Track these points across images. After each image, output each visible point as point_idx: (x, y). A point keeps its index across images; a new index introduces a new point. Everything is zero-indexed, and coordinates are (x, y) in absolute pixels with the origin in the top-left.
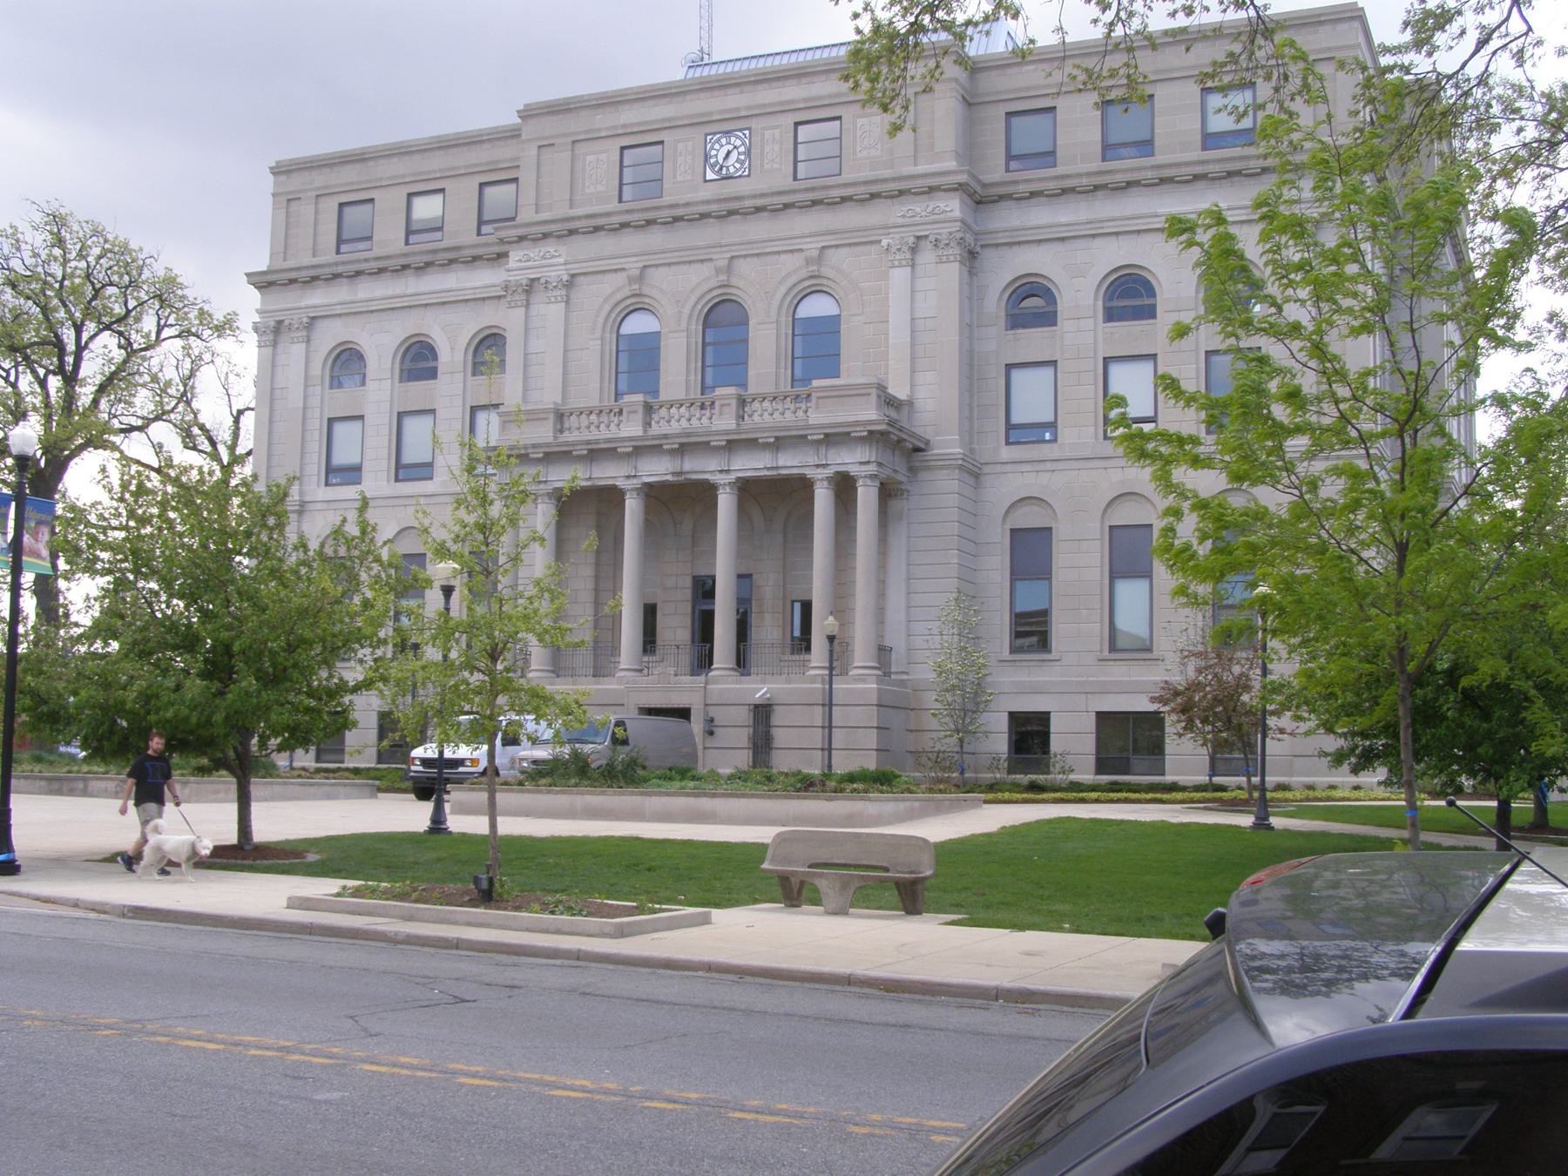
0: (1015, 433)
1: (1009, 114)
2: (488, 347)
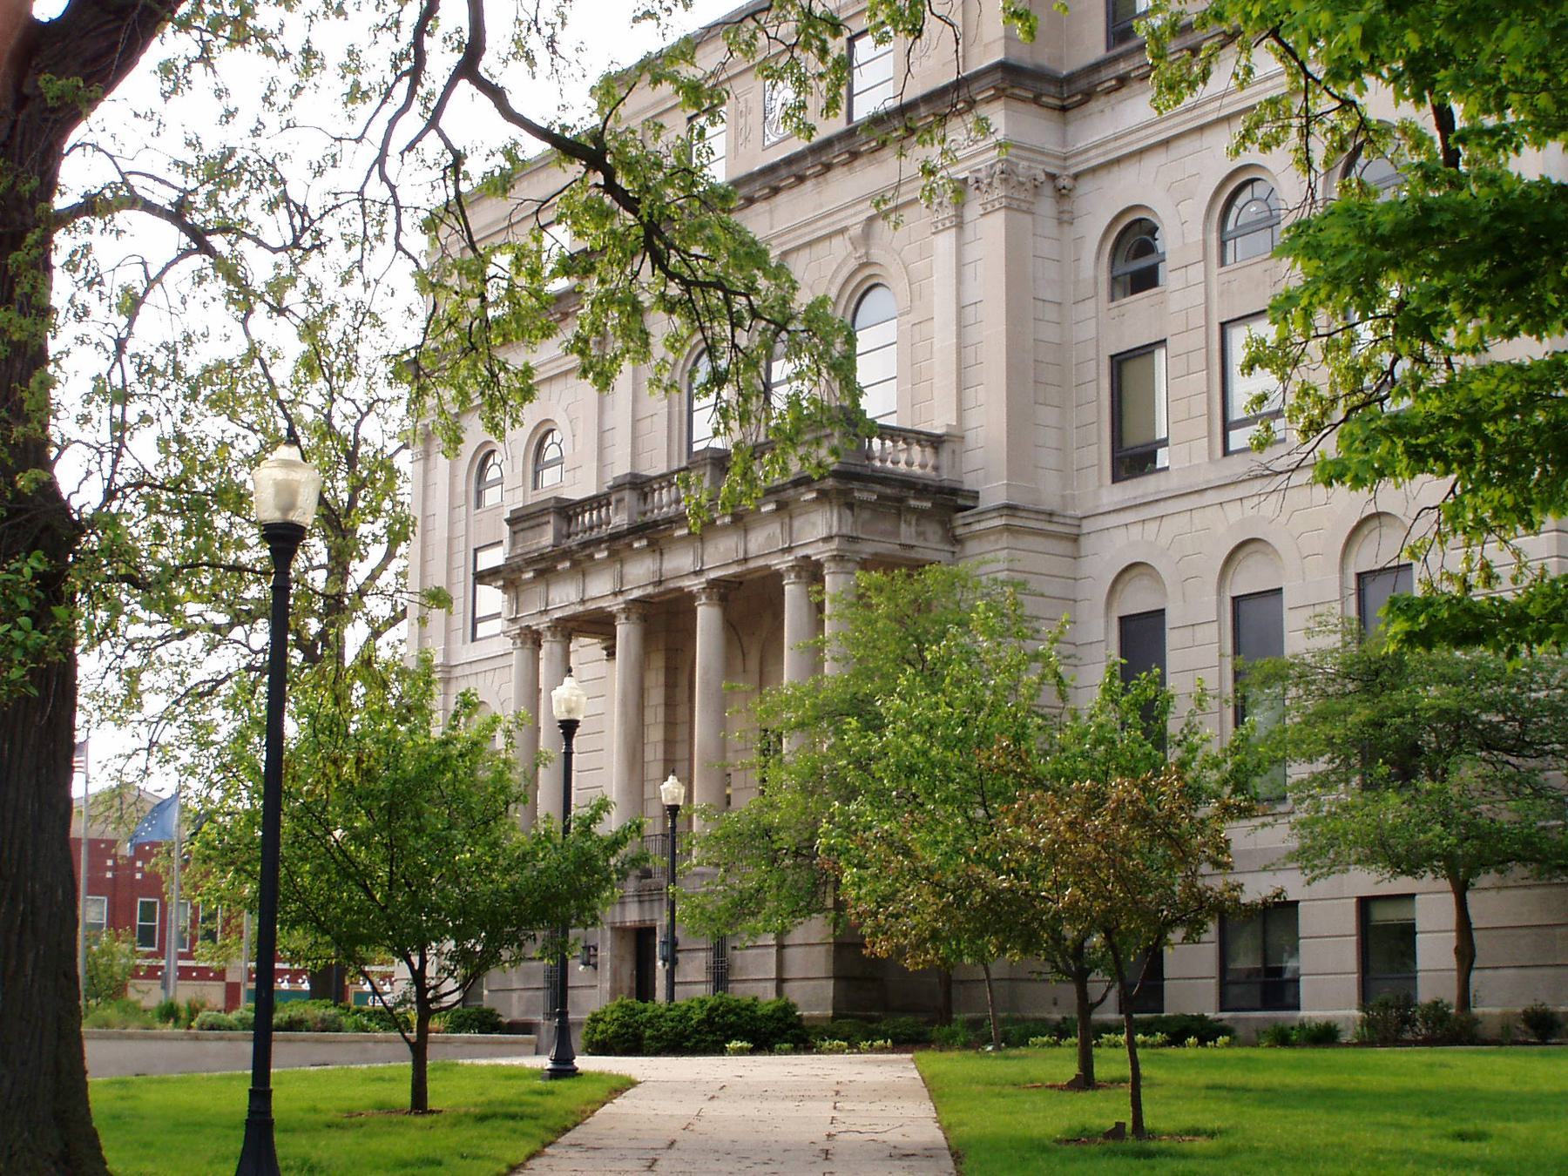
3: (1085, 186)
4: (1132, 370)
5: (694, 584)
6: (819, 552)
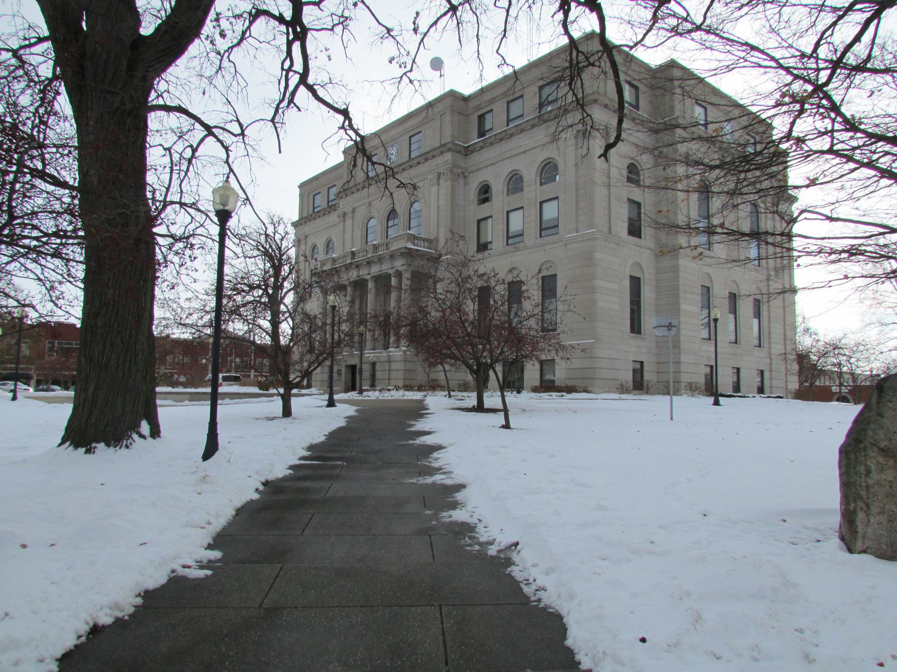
2: (548, 171)
3: (472, 175)
4: (482, 224)
5: (368, 277)
6: (401, 269)
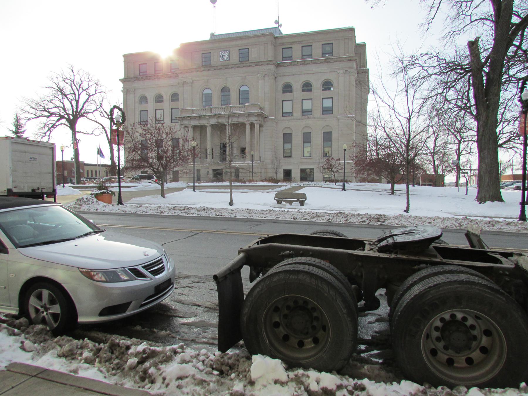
0: (285, 114)
1: (283, 49)
2: (327, 85)
